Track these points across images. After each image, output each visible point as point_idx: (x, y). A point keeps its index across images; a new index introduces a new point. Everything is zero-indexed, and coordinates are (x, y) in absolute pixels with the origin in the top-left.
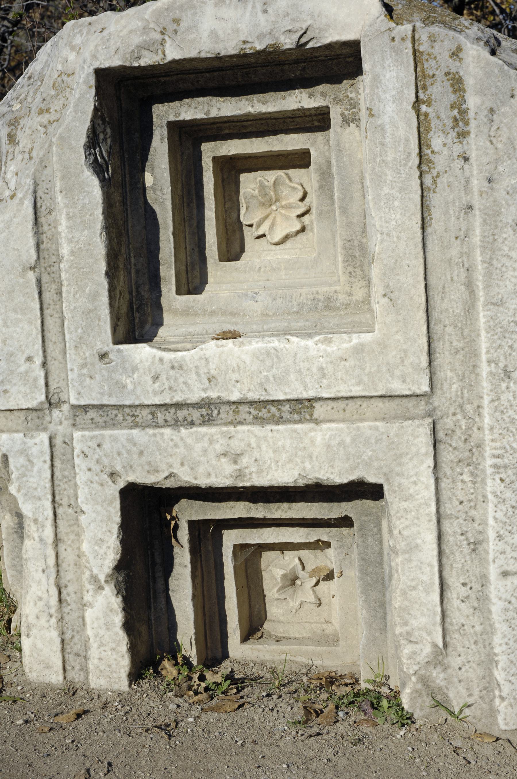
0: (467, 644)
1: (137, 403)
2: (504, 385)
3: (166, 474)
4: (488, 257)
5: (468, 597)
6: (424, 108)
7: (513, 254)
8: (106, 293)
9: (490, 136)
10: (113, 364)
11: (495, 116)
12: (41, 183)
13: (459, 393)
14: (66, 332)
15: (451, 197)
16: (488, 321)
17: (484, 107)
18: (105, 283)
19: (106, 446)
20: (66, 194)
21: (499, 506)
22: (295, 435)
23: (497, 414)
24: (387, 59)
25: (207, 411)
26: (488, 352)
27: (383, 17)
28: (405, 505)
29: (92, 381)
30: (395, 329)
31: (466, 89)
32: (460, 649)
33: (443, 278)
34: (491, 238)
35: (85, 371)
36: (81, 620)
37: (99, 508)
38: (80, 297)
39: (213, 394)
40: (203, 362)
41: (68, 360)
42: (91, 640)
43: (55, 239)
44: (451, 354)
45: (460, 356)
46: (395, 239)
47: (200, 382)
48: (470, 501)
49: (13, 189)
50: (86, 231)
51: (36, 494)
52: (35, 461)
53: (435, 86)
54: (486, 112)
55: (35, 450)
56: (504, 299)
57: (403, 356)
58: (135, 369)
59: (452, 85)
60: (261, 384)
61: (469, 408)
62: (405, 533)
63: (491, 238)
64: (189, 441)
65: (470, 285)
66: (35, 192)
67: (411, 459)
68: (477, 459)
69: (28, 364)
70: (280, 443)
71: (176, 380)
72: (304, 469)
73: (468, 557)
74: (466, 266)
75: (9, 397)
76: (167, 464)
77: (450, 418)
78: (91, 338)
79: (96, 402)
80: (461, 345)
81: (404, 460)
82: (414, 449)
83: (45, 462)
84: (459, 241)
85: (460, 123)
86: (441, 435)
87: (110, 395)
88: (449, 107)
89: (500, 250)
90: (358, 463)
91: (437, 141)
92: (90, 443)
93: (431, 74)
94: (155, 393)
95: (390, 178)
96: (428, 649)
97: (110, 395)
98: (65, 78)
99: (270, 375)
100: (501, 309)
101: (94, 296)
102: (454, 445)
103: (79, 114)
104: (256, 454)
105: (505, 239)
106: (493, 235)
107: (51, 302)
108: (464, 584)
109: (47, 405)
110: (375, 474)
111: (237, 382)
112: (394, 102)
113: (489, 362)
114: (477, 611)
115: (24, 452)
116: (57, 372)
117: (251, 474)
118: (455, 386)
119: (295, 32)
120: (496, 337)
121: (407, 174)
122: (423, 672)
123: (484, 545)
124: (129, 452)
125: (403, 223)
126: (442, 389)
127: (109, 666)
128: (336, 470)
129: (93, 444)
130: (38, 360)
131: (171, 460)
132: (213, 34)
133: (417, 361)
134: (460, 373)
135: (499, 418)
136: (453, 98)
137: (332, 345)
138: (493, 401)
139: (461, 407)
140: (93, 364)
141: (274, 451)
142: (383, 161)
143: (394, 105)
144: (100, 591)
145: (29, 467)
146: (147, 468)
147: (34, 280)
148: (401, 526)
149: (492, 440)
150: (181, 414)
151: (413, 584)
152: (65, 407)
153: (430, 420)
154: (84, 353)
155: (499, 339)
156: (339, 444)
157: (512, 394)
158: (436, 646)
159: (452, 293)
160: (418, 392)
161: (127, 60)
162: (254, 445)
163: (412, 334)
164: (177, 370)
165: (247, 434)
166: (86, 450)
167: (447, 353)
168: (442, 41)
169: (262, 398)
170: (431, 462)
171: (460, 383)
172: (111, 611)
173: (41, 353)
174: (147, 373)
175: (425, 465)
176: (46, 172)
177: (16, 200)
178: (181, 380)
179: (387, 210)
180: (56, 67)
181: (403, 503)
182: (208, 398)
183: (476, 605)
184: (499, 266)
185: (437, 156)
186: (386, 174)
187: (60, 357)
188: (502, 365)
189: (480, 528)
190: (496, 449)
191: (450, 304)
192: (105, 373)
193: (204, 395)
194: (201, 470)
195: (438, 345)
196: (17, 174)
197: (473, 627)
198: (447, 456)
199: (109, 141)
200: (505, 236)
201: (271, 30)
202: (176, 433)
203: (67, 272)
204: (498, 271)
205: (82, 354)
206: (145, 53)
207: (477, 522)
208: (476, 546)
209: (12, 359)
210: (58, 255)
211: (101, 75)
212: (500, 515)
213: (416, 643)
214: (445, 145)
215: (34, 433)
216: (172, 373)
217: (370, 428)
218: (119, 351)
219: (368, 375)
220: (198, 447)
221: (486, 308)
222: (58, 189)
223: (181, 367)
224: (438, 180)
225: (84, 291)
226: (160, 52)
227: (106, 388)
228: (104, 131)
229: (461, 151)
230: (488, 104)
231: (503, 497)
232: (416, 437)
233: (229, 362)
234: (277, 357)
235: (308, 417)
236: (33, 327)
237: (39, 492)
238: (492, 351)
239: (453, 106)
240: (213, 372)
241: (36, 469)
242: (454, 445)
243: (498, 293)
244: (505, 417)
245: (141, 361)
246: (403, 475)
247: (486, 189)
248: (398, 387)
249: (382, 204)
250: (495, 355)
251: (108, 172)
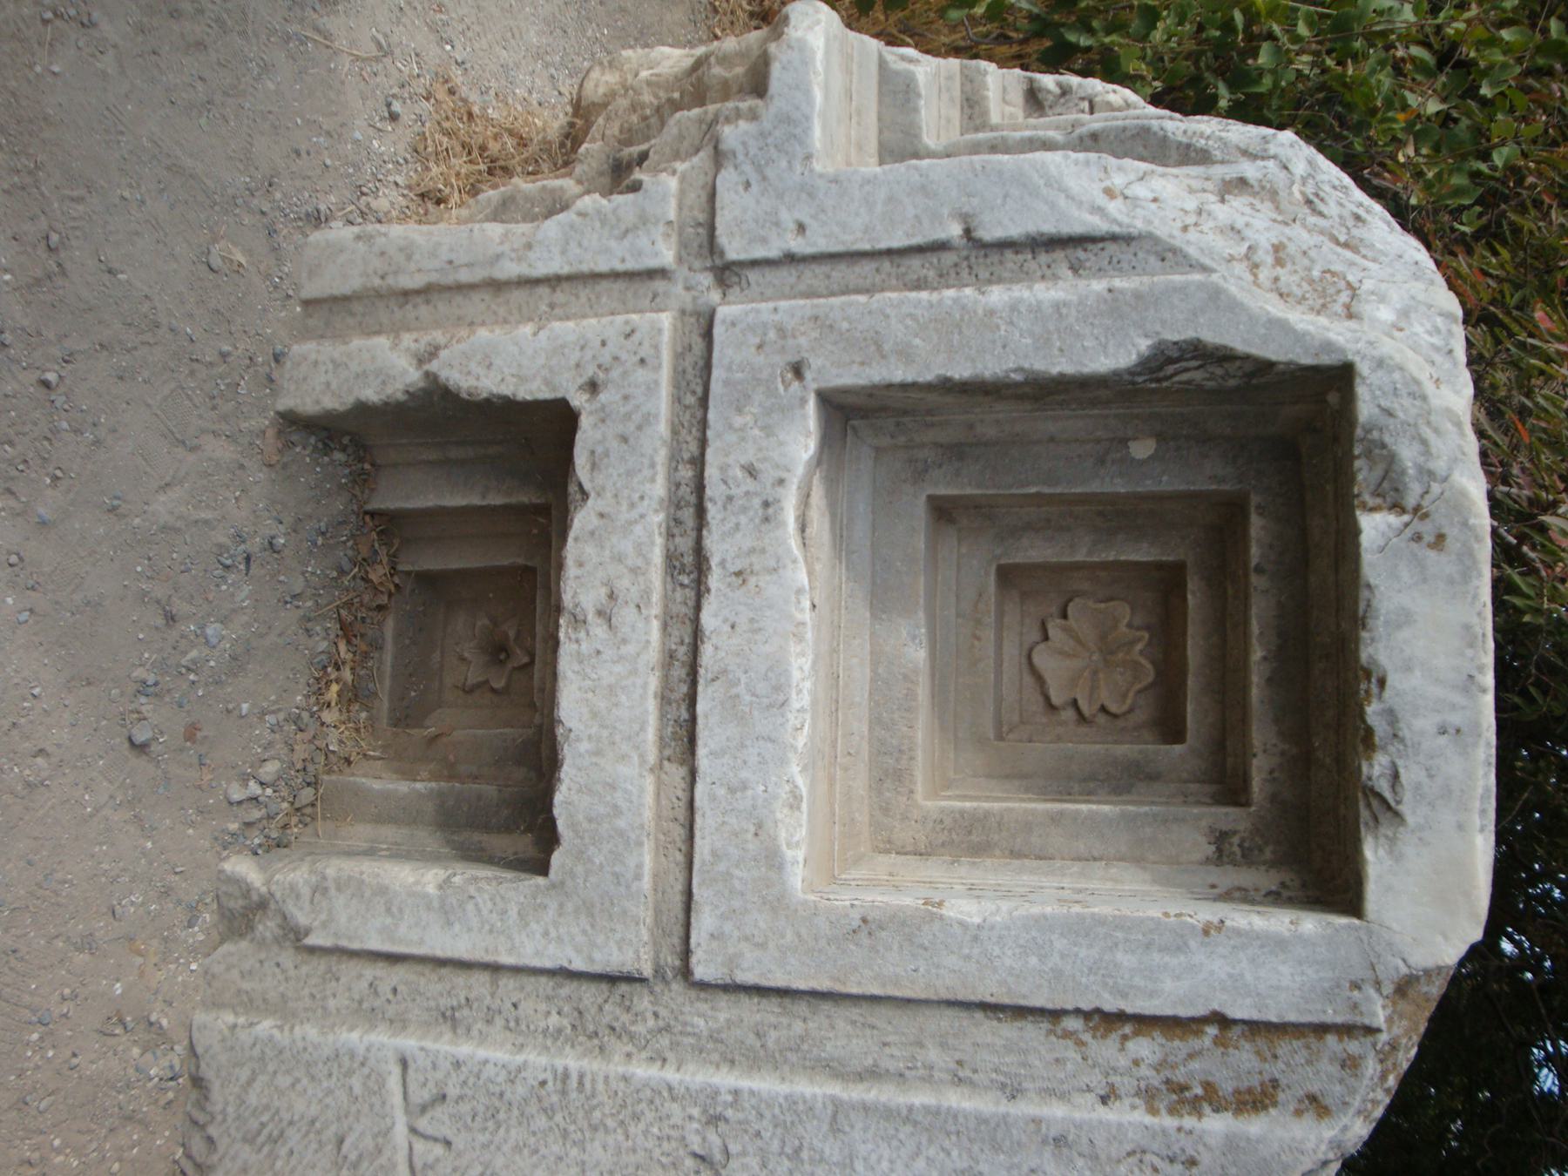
0: (313, 981)
1: (709, 433)
2: (696, 1112)
3: (587, 486)
4: (920, 1118)
5: (376, 993)
6: (1212, 1031)
7: (920, 1164)
8: (909, 379)
9: (1144, 1152)
10: (781, 388)
11: (1181, 1167)
12: (1132, 249)
13: (689, 1029)
14: (844, 298)
15: (1037, 1063)
16: (805, 1102)
17: (1201, 1148)
18: (929, 377)
19: (641, 375)
20: (1105, 301)
21: (504, 1072)
22: (636, 727)
23: (648, 1093)
24: (1317, 972)
25: (691, 569)
26: (752, 1093)
27: (1404, 970)
28: (513, 912)
29: (753, 349)
30: (803, 931)
31: (1241, 1118)
32: (304, 969)
33: (890, 1028)
34: (953, 1128)
35: (772, 335)
36: (377, 328)
37: (541, 361)
38: (907, 327)
39: (714, 580)
40: (772, 563)
41: (793, 302)
42: (343, 348)
43: (1023, 276)
44: (757, 1024)
45: (751, 1040)
46: (966, 951)
47: (738, 556)
48: (517, 1022)
49: (1128, 192)
50: (1029, 341)
51: (573, 245)
52: (626, 242)
53: (1253, 1057)
54: (1190, 1152)
55: (643, 242)
56: (841, 1135)
57: (757, 939)
58: (768, 430)
59: (1250, 1091)
60: (725, 671)
61: (665, 1041)
62: (470, 907)
63: (953, 1128)
64: (638, 529)
65: (872, 1074)
66: (1114, 238)
67: (584, 932)
68: (581, 1044)
69: (792, 226)
70: (623, 698)
71: (744, 510)
72: (578, 740)
73: (432, 1004)
74: (907, 1073)
75: (736, 192)
76: (603, 488)
77: (650, 1007)
78: (829, 347)
79: (716, 354)
80: (770, 1044)
81: (584, 922)
82: (600, 939)
83: (623, 261)
84: (953, 1065)
85: (1175, 1097)
86: (624, 988)
87: (726, 383)
88: (1210, 1079)
89: (930, 1141)
90: (582, 838)
91: (1146, 1048)
92: (646, 344)
93: (1280, 1052)
94: (723, 469)
95: (1083, 953)
96: (302, 919)
97: (726, 383)
98: (1344, 297)
99: (741, 689)
100: (825, 1127)
101: (905, 354)
102: (607, 1007)
103: (1263, 331)
104: (608, 653)
105: (949, 1154)
106: (958, 1133)
107: (903, 269)
108: (395, 991)
109: (718, 262)
110: (563, 866)
111: (733, 627)
112: (1230, 976)
113: (736, 1093)
114: (356, 1005)
115: (644, 220)
116: (776, 282)
117: (577, 641)
118: (701, 1022)
119: (1393, 787)
120: (777, 1111)
121: (1087, 987)
122: (272, 906)
123: (448, 1036)
124: (627, 417)
125: (995, 970)
126: (698, 999)
127: (305, 379)
128: (575, 798)
129: (645, 351)
130: (798, 245)
131: (609, 495)
132: (1405, 618)
133: (745, 965)
134: (723, 1036)
135: (641, 1095)
136: (1227, 1087)
137: (786, 811)
138: (670, 1089)
139: (667, 1029)
140: (783, 349)
141: (610, 687)
142: (1116, 945)
143: (1223, 976)
144: (415, 362)
145: (616, 232)
146: (599, 450)
147: (940, 235)
148: (480, 900)
149: (607, 1077)
150: (688, 515)
151: (394, 909)
152: (715, 296)
153: (647, 971)
154: (803, 334)
155: (774, 1116)
156: (615, 807)
157: (680, 1123)
158: (307, 932)
159: (861, 1042)
160: (693, 960)
161: (1368, 431)
162: (624, 650)
163: (793, 961)
164: (760, 512)
165: (647, 636)
166: (636, 337)
167: (758, 1017)
168: (1341, 1081)
169: (702, 671)
170: (579, 965)
171: (705, 1033)
172: (384, 383)
173: (809, 250)
174: (760, 455)
175: (572, 954)
176: (1152, 259)
177: (1102, 200)
178: (743, 519)
179: (1022, 942)
180: (1370, 277)
181: (516, 910)
182: (709, 568)
183: (365, 1005)
184: (902, 1136)
185: (1118, 1045)
186: (1090, 946)
187: (802, 287)
188: (729, 1113)
189: (475, 1032)
190: (593, 1081)
191: (840, 1034)
192: (765, 375)
193: (714, 562)
194: (590, 550)
195: (772, 1005)
196: (1155, 200)
197: (334, 996)
198: (590, 994)
199: (1211, 384)
200: (955, 1153)
201: (1402, 740)
202: (655, 505)
203: (955, 300)
204: (892, 1132)
205: (802, 329)
206: (1378, 472)
207: (484, 1028)
208: (449, 1019)
209: (804, 196)
210: (990, 282)
211: (1341, 377)
212: (490, 1071)
213: (312, 902)
214: (1136, 1063)
215: (674, 238)
216: (757, 502)
217: (640, 866)
218: (803, 401)
219: (728, 873)
220: (627, 546)
221: (828, 1103)
222: (1118, 283)
223: (767, 519)
224: (1070, 1043)
225: (916, 336)
226: (1379, 501)
227: (739, 375)
228: (1227, 375)
229: (1122, 1092)
230: (1205, 1159)
231: (518, 1081)
232: (620, 944)
233: (768, 613)
234: (770, 706)
235: (667, 752)
236: (859, 235)
237: (574, 249)
238: (753, 1101)
239: (1208, 1086)
240: (752, 581)
241: (613, 244)
242: (607, 1007)
243: (852, 1127)
244: (643, 1105)
245: (781, 444)
246: (560, 915)
247: (1044, 1130)
248: (704, 923)
249: (1034, 933)
250: (747, 1105)
251: (1151, 381)
